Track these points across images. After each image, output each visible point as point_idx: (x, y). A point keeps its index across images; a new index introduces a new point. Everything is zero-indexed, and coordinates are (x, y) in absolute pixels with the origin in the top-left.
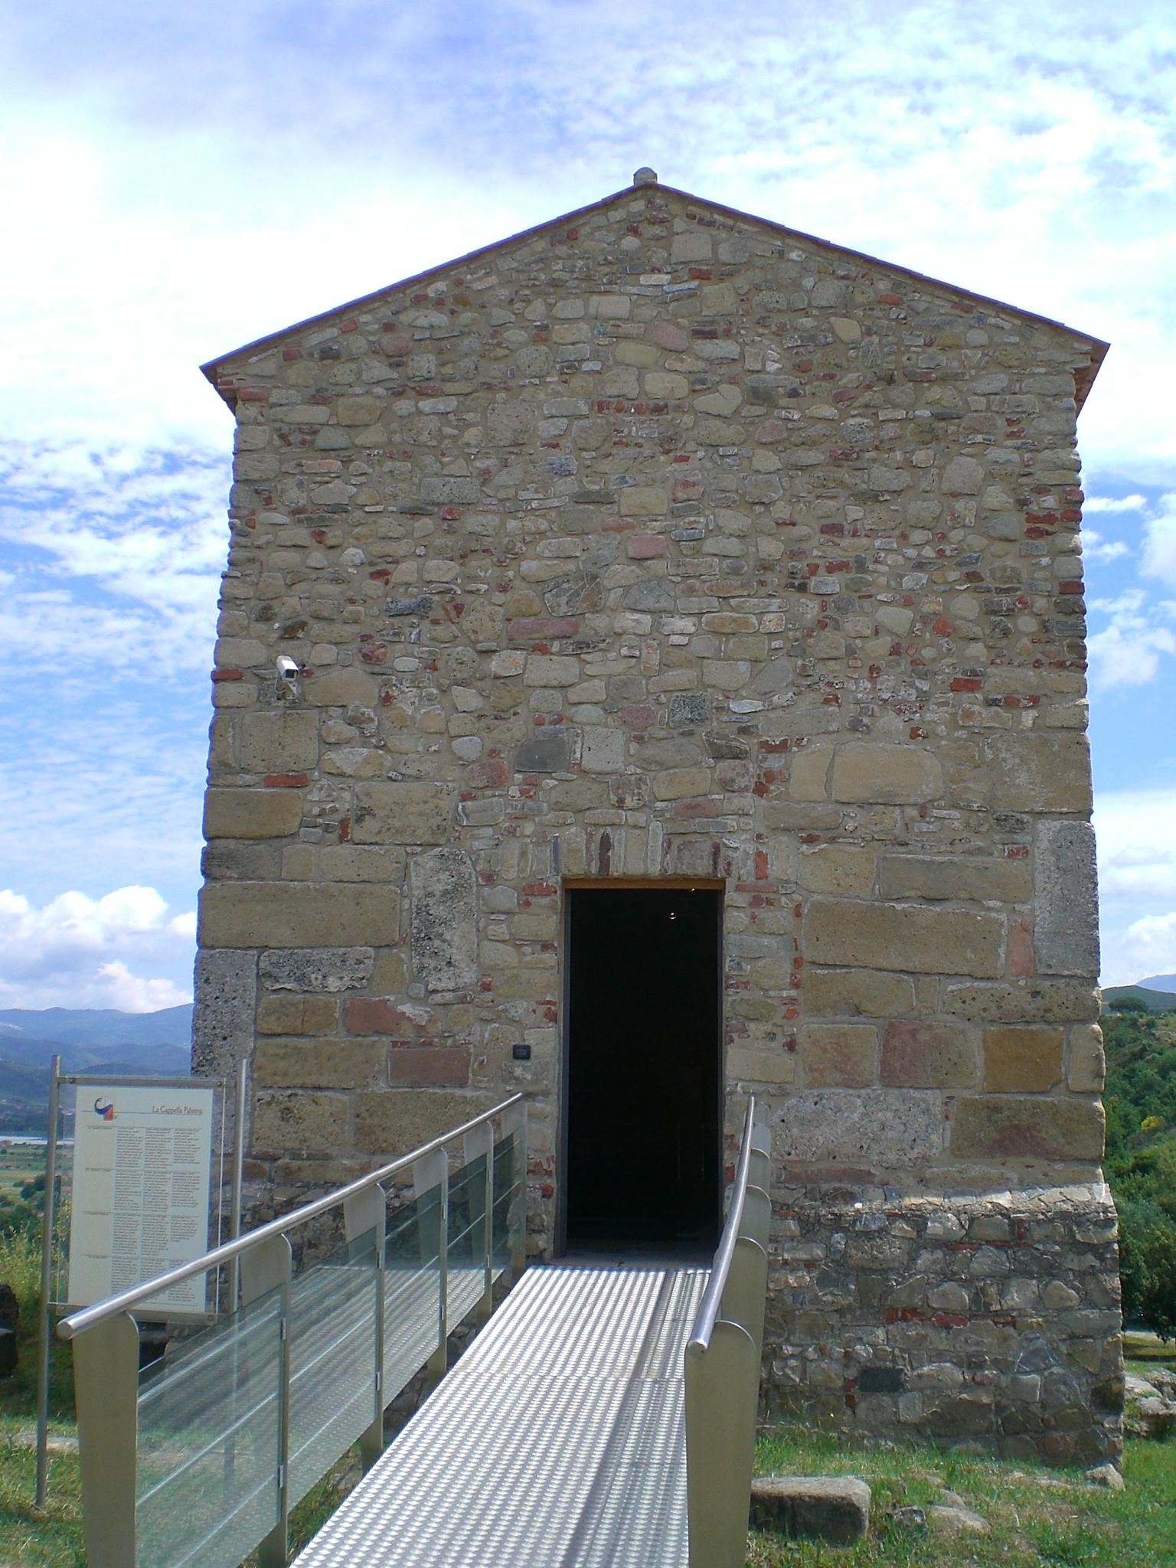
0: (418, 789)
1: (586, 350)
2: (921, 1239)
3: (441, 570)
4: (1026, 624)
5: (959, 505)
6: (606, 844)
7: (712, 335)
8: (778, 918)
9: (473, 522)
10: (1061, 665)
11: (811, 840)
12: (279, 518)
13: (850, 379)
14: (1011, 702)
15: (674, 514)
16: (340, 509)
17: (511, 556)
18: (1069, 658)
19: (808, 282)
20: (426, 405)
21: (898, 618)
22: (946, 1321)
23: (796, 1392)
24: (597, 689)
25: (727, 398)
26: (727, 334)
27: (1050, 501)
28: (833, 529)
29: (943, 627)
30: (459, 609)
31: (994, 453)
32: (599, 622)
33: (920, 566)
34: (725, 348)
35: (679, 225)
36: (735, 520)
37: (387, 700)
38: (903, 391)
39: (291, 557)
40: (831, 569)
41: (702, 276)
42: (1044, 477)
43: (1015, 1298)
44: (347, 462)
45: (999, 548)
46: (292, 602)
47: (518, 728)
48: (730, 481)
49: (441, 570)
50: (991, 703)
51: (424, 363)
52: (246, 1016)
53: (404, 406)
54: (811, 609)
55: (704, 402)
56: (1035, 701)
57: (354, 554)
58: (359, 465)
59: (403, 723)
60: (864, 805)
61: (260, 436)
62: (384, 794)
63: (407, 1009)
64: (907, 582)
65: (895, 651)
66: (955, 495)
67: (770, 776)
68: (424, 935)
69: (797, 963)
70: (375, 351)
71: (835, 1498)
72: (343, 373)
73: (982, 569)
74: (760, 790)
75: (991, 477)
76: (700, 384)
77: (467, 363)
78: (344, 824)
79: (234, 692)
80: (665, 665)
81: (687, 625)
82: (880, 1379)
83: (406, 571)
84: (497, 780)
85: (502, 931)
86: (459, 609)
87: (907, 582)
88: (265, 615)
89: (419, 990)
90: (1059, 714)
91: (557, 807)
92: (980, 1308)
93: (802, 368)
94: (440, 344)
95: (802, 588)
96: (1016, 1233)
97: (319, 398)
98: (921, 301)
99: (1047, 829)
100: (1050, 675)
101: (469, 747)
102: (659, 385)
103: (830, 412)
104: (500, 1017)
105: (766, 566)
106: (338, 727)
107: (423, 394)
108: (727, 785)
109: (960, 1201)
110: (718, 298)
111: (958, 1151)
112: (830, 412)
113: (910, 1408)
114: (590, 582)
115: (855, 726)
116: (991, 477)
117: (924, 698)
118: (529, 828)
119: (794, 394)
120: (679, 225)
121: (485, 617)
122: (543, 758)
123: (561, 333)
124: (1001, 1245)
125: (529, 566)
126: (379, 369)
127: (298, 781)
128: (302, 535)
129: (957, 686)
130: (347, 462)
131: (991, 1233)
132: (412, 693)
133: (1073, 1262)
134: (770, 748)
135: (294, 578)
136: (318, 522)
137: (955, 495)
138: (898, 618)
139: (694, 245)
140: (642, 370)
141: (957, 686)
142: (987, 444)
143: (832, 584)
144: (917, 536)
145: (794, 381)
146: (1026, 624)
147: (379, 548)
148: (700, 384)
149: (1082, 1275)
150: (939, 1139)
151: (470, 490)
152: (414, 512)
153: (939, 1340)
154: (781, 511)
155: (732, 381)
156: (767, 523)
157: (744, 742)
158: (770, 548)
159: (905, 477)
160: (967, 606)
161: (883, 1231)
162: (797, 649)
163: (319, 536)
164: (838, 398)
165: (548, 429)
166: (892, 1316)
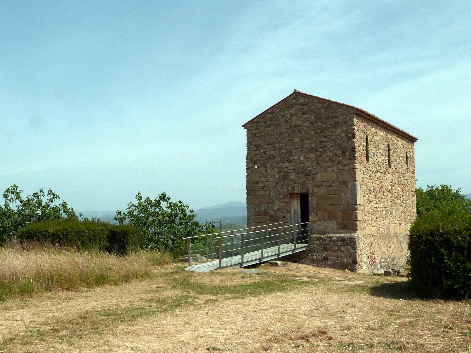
0: (271, 183)
1: (289, 118)
2: (331, 241)
3: (272, 152)
4: (347, 153)
5: (338, 137)
6: (294, 189)
7: (305, 114)
8: (315, 198)
9: (276, 145)
10: (352, 159)
11: (319, 187)
12: (252, 147)
13: (323, 119)
14: (345, 165)
15: (301, 142)
16: (259, 145)
17: (280, 150)
18: (353, 158)
19: (317, 104)
20: (269, 129)
21: (330, 154)
22: (334, 251)
23: (316, 260)
24: (291, 167)
25: (307, 124)
26: (307, 114)
27: (350, 135)
28: (321, 142)
29: (336, 155)
30: (275, 158)
31: (343, 128)
32: (292, 158)
33: (333, 146)
34: (306, 116)
35: (300, 98)
36: (308, 142)
37: (266, 171)
38: (330, 120)
39: (254, 152)
40: (321, 148)
41: (303, 105)
42: (349, 131)
43: (343, 248)
44: (260, 138)
45: (343, 143)
46: (255, 158)
47: (282, 174)
48: (307, 136)
49: (272, 152)
50: (342, 166)
51: (269, 123)
52: (253, 213)
53: (267, 129)
54: (319, 154)
55: (305, 124)
56: (348, 165)
57: (262, 151)
58: (262, 138)
59: (269, 174)
60: (326, 182)
61: (250, 135)
62: (266, 183)
63: (271, 212)
64: (331, 149)
65: (330, 159)
66: (337, 135)
67: (314, 178)
68: (272, 202)
69: (318, 204)
70: (262, 121)
71: (106, 222)
72: (259, 125)
73: (341, 146)
74: (312, 180)
75: (342, 132)
76: (303, 122)
77: (274, 122)
78: (262, 188)
79: (250, 171)
80: (300, 164)
81: (302, 157)
82: (325, 259)
83: (268, 153)
84: (280, 181)
85: (281, 201)
86: (275, 158)
87: (331, 149)
88: (252, 160)
89: (272, 209)
90: (352, 167)
91: (287, 184)
92: (338, 249)
93: (316, 118)
94: (270, 119)
95: (317, 151)
96: (343, 239)
97: (256, 129)
98: (332, 105)
99: (350, 183)
100: (351, 161)
101: (277, 177)
102: (299, 122)
103: (320, 124)
104: (282, 212)
105: (312, 148)
106: (261, 175)
107: (269, 127)
108: (308, 180)
109: (337, 235)
110: (305, 108)
111: (338, 229)
112: (320, 124)
113: (329, 262)
114: (290, 152)
115: (325, 170)
116: (342, 132)
117: (334, 166)
118: (284, 187)
119: (316, 122)
120: (300, 98)
121: (278, 158)
122: (286, 177)
123: (286, 116)
124: (341, 241)
125: (283, 151)
126: (263, 124)
127: (257, 183)
128: (255, 149)
129: (338, 164)
130: (260, 138)
131: (340, 240)
132: (269, 170)
133: (351, 244)
134: (314, 174)
135: (255, 155)
136: (257, 147)
137: (337, 135)
138: (330, 154)
139: (302, 101)
140: (296, 120)
141: (338, 164)
142: (342, 127)
143: (321, 150)
144: (332, 142)
145: (315, 120)
146: (347, 153)
147: (264, 150)
148: (303, 122)
149: (351, 245)
150: (336, 227)
151: (275, 140)
152: (269, 144)
153: (333, 254)
154: (315, 140)
155: (308, 121)
156: (313, 142)
157: (311, 174)
158: (313, 145)
159: (331, 133)
160: (339, 152)
161: (326, 239)
162: (317, 160)
163: (257, 149)
164: (322, 122)
165: (284, 131)
166: (328, 250)
